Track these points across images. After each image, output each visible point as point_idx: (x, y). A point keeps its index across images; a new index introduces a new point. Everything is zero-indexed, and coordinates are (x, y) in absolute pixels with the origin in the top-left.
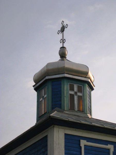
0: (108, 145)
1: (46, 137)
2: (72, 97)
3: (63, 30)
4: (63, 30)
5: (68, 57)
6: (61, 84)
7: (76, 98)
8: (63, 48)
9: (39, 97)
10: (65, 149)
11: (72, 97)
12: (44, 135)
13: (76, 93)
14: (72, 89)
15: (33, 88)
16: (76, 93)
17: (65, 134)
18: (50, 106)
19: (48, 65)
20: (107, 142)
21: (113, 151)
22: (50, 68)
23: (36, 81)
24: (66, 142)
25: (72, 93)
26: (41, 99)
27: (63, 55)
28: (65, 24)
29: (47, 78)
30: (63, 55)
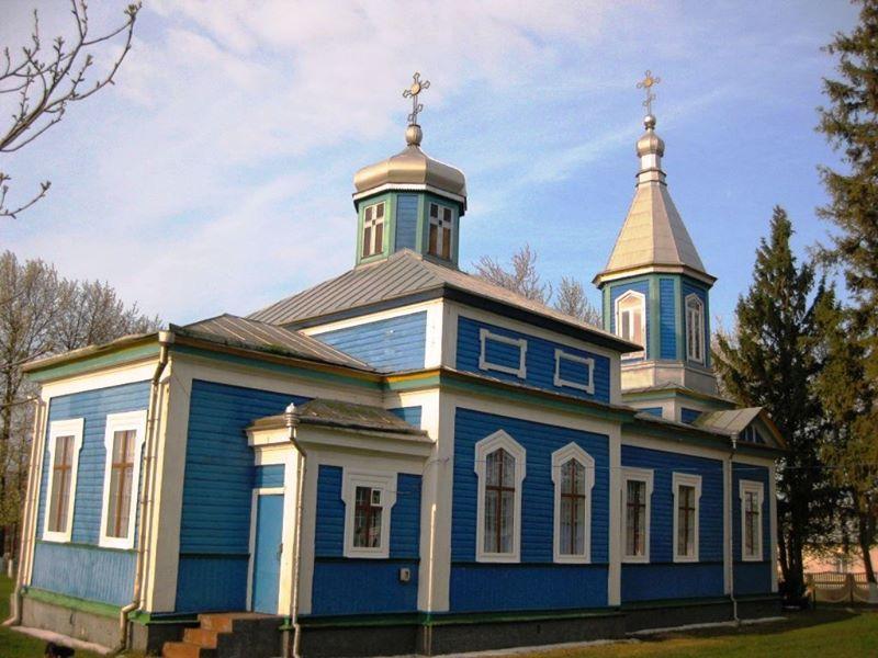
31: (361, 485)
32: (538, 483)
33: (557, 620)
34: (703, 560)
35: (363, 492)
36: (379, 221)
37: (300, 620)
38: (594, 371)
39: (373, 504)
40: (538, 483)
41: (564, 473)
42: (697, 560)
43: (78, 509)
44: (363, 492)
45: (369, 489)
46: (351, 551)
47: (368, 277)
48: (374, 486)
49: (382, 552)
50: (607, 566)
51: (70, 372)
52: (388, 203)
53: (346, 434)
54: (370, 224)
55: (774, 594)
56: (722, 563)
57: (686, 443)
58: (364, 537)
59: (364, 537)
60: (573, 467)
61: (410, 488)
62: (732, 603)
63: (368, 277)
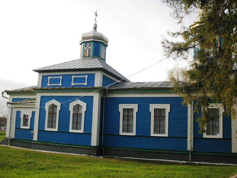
27: (95, 28)
30: (95, 28)
31: (25, 114)
32: (65, 111)
33: (68, 147)
34: (138, 134)
35: (25, 116)
36: (89, 48)
37: (192, 151)
38: (72, 82)
39: (27, 118)
40: (65, 111)
41: (74, 109)
42: (221, 137)
43: (137, 116)
44: (25, 116)
45: (26, 115)
46: (22, 127)
47: (87, 61)
48: (27, 114)
49: (28, 127)
50: (91, 134)
51: (70, 91)
52: (92, 44)
53: (18, 105)
54: (86, 48)
55: (35, 141)
56: (187, 138)
57: (163, 93)
58: (51, 126)
59: (51, 126)
60: (78, 107)
61: (33, 113)
62: (102, 149)
63: (87, 61)
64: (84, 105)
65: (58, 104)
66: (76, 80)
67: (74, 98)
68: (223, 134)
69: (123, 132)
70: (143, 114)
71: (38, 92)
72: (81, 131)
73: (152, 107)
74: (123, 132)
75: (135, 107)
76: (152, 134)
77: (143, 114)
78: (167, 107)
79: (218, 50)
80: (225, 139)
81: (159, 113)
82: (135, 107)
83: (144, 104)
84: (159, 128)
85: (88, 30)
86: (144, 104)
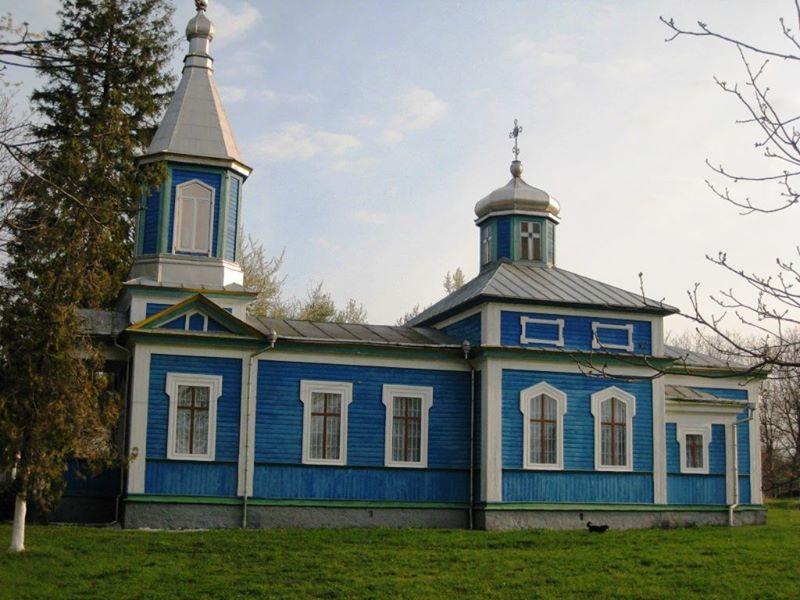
0: (480, 372)
1: (480, 314)
2: (525, 240)
3: (516, 132)
4: (516, 132)
5: (523, 176)
6: (509, 223)
7: (530, 242)
8: (516, 162)
9: (482, 234)
10: (502, 330)
11: (525, 240)
12: (476, 312)
13: (531, 235)
14: (525, 229)
15: (474, 223)
16: (531, 235)
17: (502, 312)
18: (495, 255)
19: (494, 194)
20: (530, 344)
21: (431, 404)
22: (495, 199)
23: (479, 213)
24: (502, 321)
25: (525, 235)
26: (485, 241)
27: (516, 173)
28: (519, 125)
29: (492, 214)
30: (516, 173)
58: (192, 439)
64: (629, 400)
65: (561, 400)
66: (533, 330)
67: (534, 377)
68: (217, 451)
69: (603, 463)
70: (367, 410)
71: (494, 357)
72: (557, 465)
73: (391, 393)
74: (603, 463)
75: (345, 391)
76: (307, 459)
77: (367, 410)
78: (426, 395)
79: (42, 203)
80: (353, 467)
81: (408, 409)
82: (345, 391)
83: (367, 386)
84: (408, 448)
85: (492, 181)
86: (367, 386)
